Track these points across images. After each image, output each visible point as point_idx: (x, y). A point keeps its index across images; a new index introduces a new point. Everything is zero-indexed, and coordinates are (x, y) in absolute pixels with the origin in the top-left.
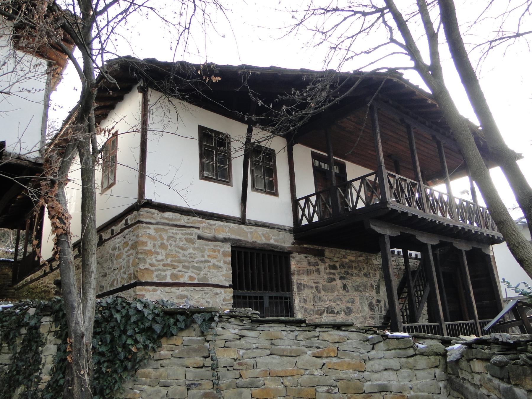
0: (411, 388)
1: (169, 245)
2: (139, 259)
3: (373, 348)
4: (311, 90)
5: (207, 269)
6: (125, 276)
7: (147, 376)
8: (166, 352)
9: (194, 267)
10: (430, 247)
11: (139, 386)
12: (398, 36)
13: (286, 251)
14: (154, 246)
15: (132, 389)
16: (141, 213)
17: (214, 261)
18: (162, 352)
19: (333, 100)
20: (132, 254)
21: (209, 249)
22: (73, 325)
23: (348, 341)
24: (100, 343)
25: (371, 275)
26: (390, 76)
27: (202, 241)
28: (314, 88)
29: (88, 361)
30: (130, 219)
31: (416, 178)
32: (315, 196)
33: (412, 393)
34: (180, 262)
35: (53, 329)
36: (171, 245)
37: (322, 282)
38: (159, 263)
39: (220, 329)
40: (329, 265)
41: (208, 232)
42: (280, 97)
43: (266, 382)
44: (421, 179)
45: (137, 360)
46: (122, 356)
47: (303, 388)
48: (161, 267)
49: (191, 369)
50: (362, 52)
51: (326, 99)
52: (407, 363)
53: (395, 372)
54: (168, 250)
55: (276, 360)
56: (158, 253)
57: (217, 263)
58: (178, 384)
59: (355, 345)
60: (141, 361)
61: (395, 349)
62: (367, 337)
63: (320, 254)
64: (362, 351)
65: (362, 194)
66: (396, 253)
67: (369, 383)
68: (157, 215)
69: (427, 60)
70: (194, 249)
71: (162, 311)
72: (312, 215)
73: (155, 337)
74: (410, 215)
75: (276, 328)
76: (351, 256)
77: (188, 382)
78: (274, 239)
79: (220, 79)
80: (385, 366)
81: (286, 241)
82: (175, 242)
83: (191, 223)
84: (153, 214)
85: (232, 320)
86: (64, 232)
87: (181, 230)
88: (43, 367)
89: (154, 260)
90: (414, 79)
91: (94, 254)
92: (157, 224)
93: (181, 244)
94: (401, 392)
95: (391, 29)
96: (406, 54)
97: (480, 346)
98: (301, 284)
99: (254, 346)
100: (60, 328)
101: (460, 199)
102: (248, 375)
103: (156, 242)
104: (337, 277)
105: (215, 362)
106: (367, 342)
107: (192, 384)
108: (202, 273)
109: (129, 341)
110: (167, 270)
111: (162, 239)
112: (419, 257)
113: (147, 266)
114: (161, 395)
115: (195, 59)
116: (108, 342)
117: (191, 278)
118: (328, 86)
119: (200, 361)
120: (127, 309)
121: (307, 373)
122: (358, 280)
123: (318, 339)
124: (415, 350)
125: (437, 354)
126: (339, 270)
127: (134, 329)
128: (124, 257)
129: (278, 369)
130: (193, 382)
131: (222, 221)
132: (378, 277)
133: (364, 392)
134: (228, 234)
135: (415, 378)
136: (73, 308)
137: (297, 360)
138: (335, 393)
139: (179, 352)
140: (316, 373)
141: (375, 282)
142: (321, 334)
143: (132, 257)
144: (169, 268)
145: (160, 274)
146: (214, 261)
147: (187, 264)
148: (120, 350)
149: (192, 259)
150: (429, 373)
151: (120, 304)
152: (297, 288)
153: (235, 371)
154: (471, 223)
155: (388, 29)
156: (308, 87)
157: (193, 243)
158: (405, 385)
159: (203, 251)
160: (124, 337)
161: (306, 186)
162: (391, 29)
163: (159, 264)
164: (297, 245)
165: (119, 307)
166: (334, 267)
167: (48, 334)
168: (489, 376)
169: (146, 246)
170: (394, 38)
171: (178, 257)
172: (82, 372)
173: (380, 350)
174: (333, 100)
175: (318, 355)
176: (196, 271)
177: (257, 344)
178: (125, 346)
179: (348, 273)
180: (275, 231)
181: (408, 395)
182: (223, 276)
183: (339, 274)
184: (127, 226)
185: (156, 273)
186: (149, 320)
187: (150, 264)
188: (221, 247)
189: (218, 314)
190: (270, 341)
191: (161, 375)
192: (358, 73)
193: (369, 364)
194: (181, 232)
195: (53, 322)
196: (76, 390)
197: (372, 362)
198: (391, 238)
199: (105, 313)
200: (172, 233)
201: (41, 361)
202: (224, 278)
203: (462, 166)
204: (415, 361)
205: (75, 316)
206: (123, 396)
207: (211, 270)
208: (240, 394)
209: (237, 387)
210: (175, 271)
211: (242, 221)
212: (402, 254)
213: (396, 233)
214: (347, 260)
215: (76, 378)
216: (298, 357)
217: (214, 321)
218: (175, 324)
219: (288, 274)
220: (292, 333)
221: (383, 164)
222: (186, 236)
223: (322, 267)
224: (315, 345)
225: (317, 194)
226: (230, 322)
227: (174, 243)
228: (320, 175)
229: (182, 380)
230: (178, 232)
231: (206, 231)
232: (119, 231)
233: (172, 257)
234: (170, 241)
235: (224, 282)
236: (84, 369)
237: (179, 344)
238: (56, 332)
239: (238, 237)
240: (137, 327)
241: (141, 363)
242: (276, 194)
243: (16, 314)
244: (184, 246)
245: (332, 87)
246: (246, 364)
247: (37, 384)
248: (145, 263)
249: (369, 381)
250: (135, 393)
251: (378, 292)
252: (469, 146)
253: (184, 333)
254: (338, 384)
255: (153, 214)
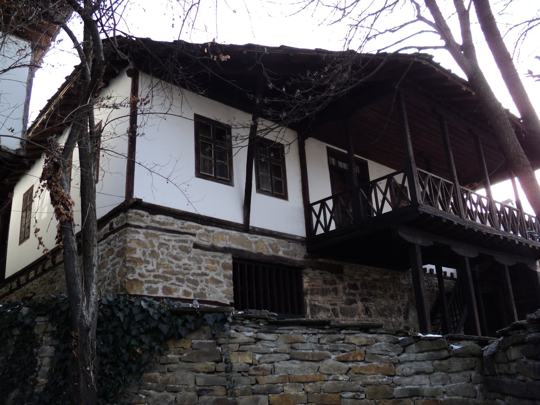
0: (444, 393)
1: (160, 253)
2: (127, 268)
3: (404, 352)
4: (330, 71)
5: (204, 283)
6: (111, 288)
7: (154, 380)
8: (173, 356)
9: (189, 280)
10: (467, 261)
11: (144, 390)
12: (426, 13)
13: (297, 265)
14: (144, 254)
15: (136, 394)
16: (130, 215)
17: (212, 274)
18: (169, 356)
19: (355, 82)
20: (118, 263)
21: (206, 260)
22: (79, 318)
23: (377, 344)
24: (102, 343)
25: (399, 297)
26: (419, 58)
27: (198, 251)
28: (332, 70)
29: (93, 359)
30: (116, 223)
31: (452, 179)
32: (331, 200)
33: (446, 397)
34: (173, 273)
35: (50, 328)
36: (162, 254)
37: (340, 305)
38: (149, 273)
39: (233, 331)
40: (349, 284)
41: (206, 240)
42: (293, 80)
43: (285, 388)
44: (456, 179)
45: (143, 363)
46: (126, 357)
47: (326, 394)
48: (151, 278)
49: (202, 374)
50: (386, 31)
51: (348, 81)
52: (441, 365)
53: (428, 376)
54: (159, 260)
55: (296, 365)
56: (148, 262)
57: (216, 277)
58: (187, 390)
59: (384, 347)
60: (146, 364)
61: (428, 351)
62: (397, 339)
63: (338, 271)
64: (392, 354)
65: (388, 196)
66: (428, 271)
67: (400, 388)
68: (147, 219)
69: (459, 40)
70: (189, 259)
71: (168, 311)
72: (327, 222)
73: (162, 338)
74: (444, 221)
75: (296, 331)
76: (375, 274)
77: (198, 388)
78: (283, 251)
79: (229, 57)
80: (415, 372)
81: (298, 254)
82: (167, 249)
83: (186, 228)
84: (143, 216)
85: (247, 322)
86: (68, 219)
87: (175, 236)
88: (39, 369)
89: (144, 270)
90: (446, 61)
91: (95, 246)
92: (147, 228)
93: (175, 252)
94: (433, 397)
95: (418, 7)
96: (435, 32)
97: (517, 331)
98: (315, 305)
99: (272, 350)
100: (57, 328)
101: (501, 204)
102: (265, 381)
103: (145, 250)
104: (358, 298)
105: (229, 365)
106: (398, 345)
107: (203, 390)
108: (199, 287)
109: (133, 342)
110: (159, 282)
111: (153, 246)
112: (455, 276)
113: (136, 276)
114: (169, 401)
115: (197, 37)
116: (111, 343)
117: (186, 293)
118: (350, 67)
119: (210, 365)
120: (131, 309)
121: (331, 378)
122: (383, 303)
123: (343, 343)
124: (449, 351)
125: (473, 355)
126: (360, 291)
127: (139, 329)
128: (109, 266)
129: (298, 374)
130: (203, 388)
131: (222, 228)
132: (406, 299)
133: (394, 398)
134: (228, 243)
135: (449, 381)
136: (78, 300)
137: (320, 365)
138: (362, 399)
139: (188, 355)
140: (340, 379)
141: (402, 305)
142: (347, 336)
143: (118, 266)
144: (160, 280)
145: (151, 287)
146: (212, 274)
147: (181, 277)
148: (124, 351)
149: (186, 271)
150: (465, 376)
151: (123, 302)
152: (311, 310)
153: (250, 377)
154: (515, 233)
155: (415, 6)
156: (326, 69)
157: (188, 252)
158: (438, 388)
159: (199, 262)
160: (128, 338)
161: (321, 188)
162: (418, 7)
163: (150, 275)
164: (310, 260)
165: (121, 306)
166: (354, 287)
167: (44, 335)
168: (524, 359)
169: (135, 253)
170: (422, 15)
171: (171, 267)
172: (88, 369)
173: (410, 354)
174: (355, 82)
175: (343, 359)
176: (191, 285)
177: (275, 348)
178: (129, 347)
179: (370, 294)
180: (285, 242)
181: (442, 399)
182: (223, 292)
183: (360, 295)
184: (112, 231)
185: (146, 285)
186: (155, 320)
187: (140, 275)
188: (220, 258)
189: (231, 315)
190: (290, 345)
191: (168, 380)
192: (381, 57)
193: (400, 367)
194: (174, 238)
195: (49, 321)
196: (82, 386)
197: (402, 366)
198: (423, 248)
199: (106, 312)
200: (164, 239)
201: (37, 363)
202: (225, 295)
203: (504, 169)
204: (449, 363)
205: (80, 308)
206: (128, 401)
207: (210, 285)
208: (257, 400)
209: (253, 394)
210: (167, 284)
211: (245, 227)
212: (435, 272)
213: (428, 243)
214: (370, 279)
215: (82, 374)
216: (321, 362)
217: (228, 321)
218: (184, 325)
219: (300, 293)
220: (314, 336)
221: (413, 160)
222: (180, 244)
223: (340, 287)
224: (340, 349)
225: (333, 197)
226: (244, 325)
227: (166, 251)
228: (337, 176)
229: (192, 385)
230: (171, 238)
231: (203, 238)
232: (102, 237)
233: (164, 268)
234: (162, 249)
235: (225, 299)
236: (89, 365)
237: (188, 347)
238: (52, 332)
239: (240, 247)
240: (142, 327)
241: (147, 367)
242: (285, 197)
243: (7, 314)
244: (178, 255)
245: (355, 67)
246: (263, 369)
247: (33, 387)
248: (134, 272)
249: (399, 385)
250: (141, 398)
251: (406, 318)
252: (506, 132)
253: (193, 336)
254: (365, 389)
255: (143, 216)
